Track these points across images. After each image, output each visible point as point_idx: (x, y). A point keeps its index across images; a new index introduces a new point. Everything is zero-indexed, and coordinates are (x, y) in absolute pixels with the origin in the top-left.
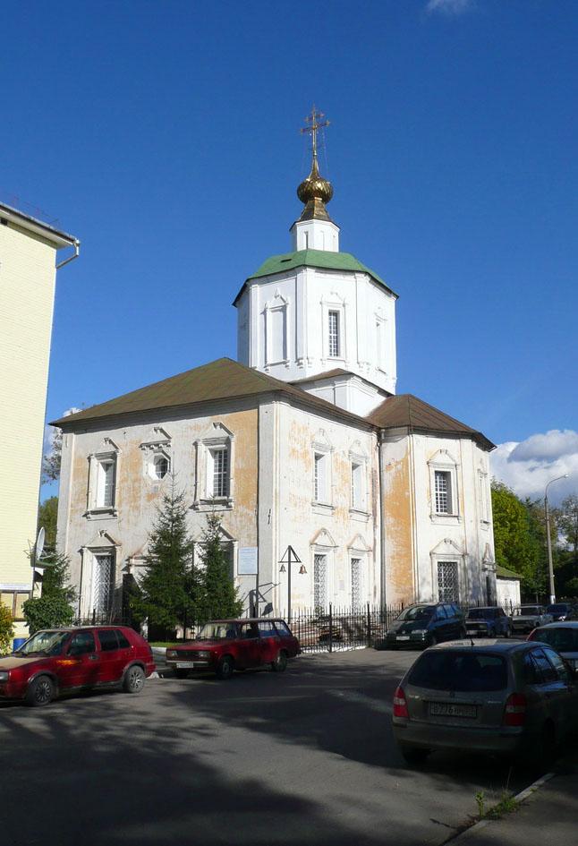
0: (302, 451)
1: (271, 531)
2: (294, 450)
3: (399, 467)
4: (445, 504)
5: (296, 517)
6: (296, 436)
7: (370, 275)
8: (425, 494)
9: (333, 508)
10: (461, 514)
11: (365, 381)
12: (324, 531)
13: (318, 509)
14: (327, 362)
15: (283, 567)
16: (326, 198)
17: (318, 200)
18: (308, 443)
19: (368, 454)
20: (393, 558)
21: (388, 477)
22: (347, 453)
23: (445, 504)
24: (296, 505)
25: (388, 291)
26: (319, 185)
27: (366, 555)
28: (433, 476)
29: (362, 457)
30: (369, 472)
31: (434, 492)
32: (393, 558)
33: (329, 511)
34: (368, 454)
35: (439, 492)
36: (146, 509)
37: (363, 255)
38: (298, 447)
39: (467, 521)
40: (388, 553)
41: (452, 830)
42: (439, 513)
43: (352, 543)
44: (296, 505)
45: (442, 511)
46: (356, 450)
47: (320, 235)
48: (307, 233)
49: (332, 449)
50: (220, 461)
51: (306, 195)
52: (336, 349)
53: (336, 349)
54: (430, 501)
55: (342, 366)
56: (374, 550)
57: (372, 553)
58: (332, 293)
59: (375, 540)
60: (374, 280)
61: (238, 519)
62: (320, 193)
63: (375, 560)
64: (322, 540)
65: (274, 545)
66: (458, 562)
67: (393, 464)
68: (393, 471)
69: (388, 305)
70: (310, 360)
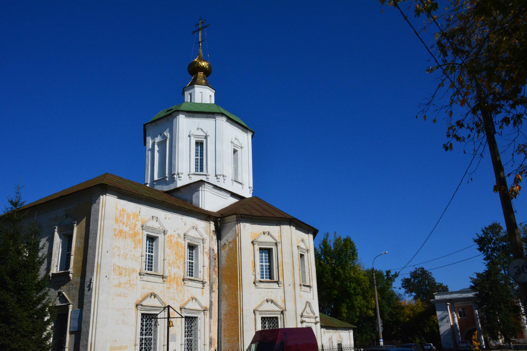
0: (132, 232)
1: (91, 295)
2: (121, 232)
3: (231, 245)
4: (270, 274)
5: (120, 284)
6: (125, 220)
7: (226, 116)
8: (251, 265)
9: (163, 277)
10: (281, 280)
11: (216, 187)
12: (153, 295)
13: (146, 278)
14: (192, 176)
16: (207, 72)
17: (201, 74)
18: (139, 227)
19: (206, 236)
20: (226, 315)
21: (224, 253)
22: (182, 236)
23: (270, 274)
25: (245, 129)
26: (204, 64)
27: (202, 313)
28: (257, 253)
29: (199, 239)
31: (258, 264)
32: (226, 315)
33: (160, 280)
34: (206, 236)
35: (148, 253)
36: (169, 288)
37: (229, 107)
38: (126, 229)
40: (223, 312)
43: (186, 304)
45: (148, 270)
46: (302, 245)
47: (203, 95)
48: (191, 94)
49: (165, 232)
51: (194, 69)
52: (200, 165)
53: (200, 165)
54: (255, 270)
55: (204, 178)
56: (211, 309)
57: (208, 313)
59: (211, 302)
60: (229, 119)
62: (202, 69)
63: (211, 317)
66: (279, 316)
68: (227, 249)
69: (245, 139)
70: (180, 175)
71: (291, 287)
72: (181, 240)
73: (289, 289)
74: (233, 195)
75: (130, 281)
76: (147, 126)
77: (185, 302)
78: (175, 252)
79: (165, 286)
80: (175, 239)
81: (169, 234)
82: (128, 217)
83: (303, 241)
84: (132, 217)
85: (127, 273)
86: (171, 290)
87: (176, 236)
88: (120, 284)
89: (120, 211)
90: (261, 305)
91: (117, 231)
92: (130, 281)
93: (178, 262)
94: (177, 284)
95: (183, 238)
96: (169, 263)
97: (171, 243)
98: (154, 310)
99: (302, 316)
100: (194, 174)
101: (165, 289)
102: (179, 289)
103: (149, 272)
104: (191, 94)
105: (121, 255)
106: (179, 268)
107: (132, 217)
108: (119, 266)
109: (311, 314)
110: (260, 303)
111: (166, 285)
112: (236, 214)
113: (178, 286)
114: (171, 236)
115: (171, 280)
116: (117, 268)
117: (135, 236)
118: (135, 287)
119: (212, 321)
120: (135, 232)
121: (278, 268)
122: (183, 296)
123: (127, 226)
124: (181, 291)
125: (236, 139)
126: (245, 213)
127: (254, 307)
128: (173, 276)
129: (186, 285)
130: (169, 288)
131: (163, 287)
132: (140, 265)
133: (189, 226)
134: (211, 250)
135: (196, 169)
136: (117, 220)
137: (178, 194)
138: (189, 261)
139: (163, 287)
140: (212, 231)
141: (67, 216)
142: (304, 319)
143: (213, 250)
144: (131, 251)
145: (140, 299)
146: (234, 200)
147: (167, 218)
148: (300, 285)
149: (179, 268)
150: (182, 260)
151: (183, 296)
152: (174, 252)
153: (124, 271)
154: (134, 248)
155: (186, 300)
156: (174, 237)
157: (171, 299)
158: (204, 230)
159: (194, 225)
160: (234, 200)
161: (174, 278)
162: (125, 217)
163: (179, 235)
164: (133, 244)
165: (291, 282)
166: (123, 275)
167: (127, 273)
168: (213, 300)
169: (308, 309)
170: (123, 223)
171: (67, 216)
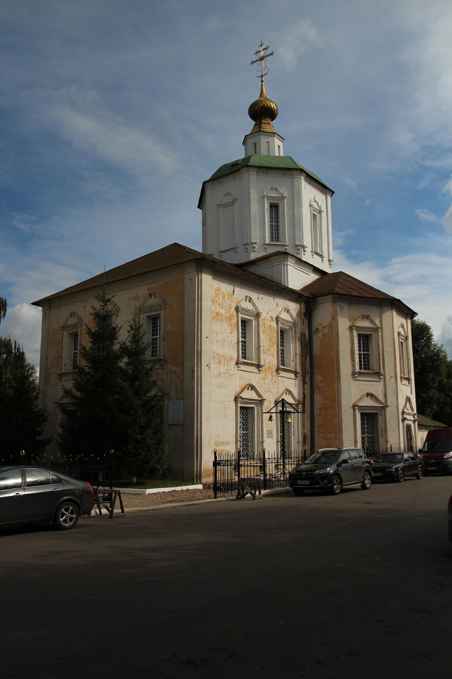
0: (227, 315)
2: (217, 314)
3: (326, 330)
5: (220, 374)
6: (220, 301)
9: (258, 366)
12: (252, 387)
13: (243, 367)
15: (271, 417)
23: (246, 355)
24: (220, 362)
30: (298, 335)
33: (254, 369)
35: (362, 352)
38: (222, 311)
39: (387, 377)
41: (393, 311)
42: (362, 371)
44: (220, 362)
45: (365, 369)
48: (255, 144)
49: (258, 315)
50: (304, 382)
53: (276, 233)
58: (272, 189)
59: (304, 395)
61: (169, 376)
64: (249, 394)
65: (368, 412)
67: (320, 328)
71: (393, 379)
72: (274, 324)
73: (390, 382)
74: (316, 270)
75: (228, 370)
76: (207, 185)
77: (279, 395)
78: (269, 338)
79: (261, 377)
80: (268, 322)
81: (262, 316)
82: (224, 297)
83: (402, 326)
84: (226, 297)
85: (226, 362)
86: (267, 381)
87: (269, 319)
88: (220, 374)
89: (216, 290)
90: (360, 399)
91: (214, 313)
92: (228, 370)
93: (272, 349)
94: (272, 374)
95: (275, 322)
96: (264, 352)
97: (265, 327)
98: (252, 403)
99: (403, 413)
100: (268, 245)
101: (261, 380)
102: (274, 381)
103: (368, 371)
104: (255, 144)
105: (219, 341)
106: (273, 356)
107: (226, 297)
108: (217, 354)
109: (410, 411)
110: (359, 397)
111: (262, 375)
112: (332, 294)
113: (273, 376)
114: (264, 319)
115: (266, 370)
116: (216, 356)
117: (231, 320)
118: (233, 377)
119: (305, 415)
120: (230, 314)
121: (408, 361)
122: (278, 388)
123: (222, 308)
124: (275, 382)
125: (315, 201)
126: (343, 293)
127: (353, 401)
128: (267, 366)
129: (280, 375)
130: (264, 379)
131: (259, 377)
132: (233, 352)
133: (280, 308)
134: (303, 336)
135: (272, 238)
136: (213, 301)
137: (254, 269)
138: (158, 336)
139: (259, 377)
140: (303, 313)
141: (150, 295)
142: (406, 416)
143: (305, 335)
144: (228, 337)
145: (238, 390)
146: (313, 277)
147: (260, 299)
148: (401, 378)
149: (273, 356)
150: (275, 346)
151: (278, 388)
152: (268, 338)
153: (223, 359)
154: (231, 333)
155: (281, 392)
156: (267, 320)
157: (267, 391)
158: (288, 310)
159: (286, 306)
160: (313, 277)
161: (269, 368)
162: (221, 297)
163: (271, 317)
164: (229, 327)
165: (393, 374)
166: (222, 363)
167: (226, 362)
168: (306, 392)
169: (408, 405)
170: (219, 305)
171: (150, 295)
